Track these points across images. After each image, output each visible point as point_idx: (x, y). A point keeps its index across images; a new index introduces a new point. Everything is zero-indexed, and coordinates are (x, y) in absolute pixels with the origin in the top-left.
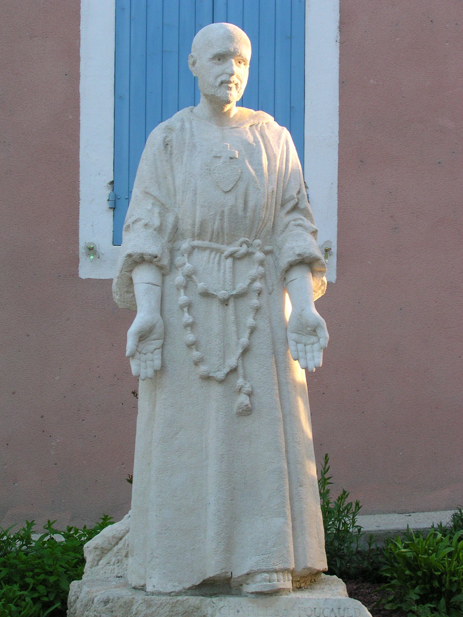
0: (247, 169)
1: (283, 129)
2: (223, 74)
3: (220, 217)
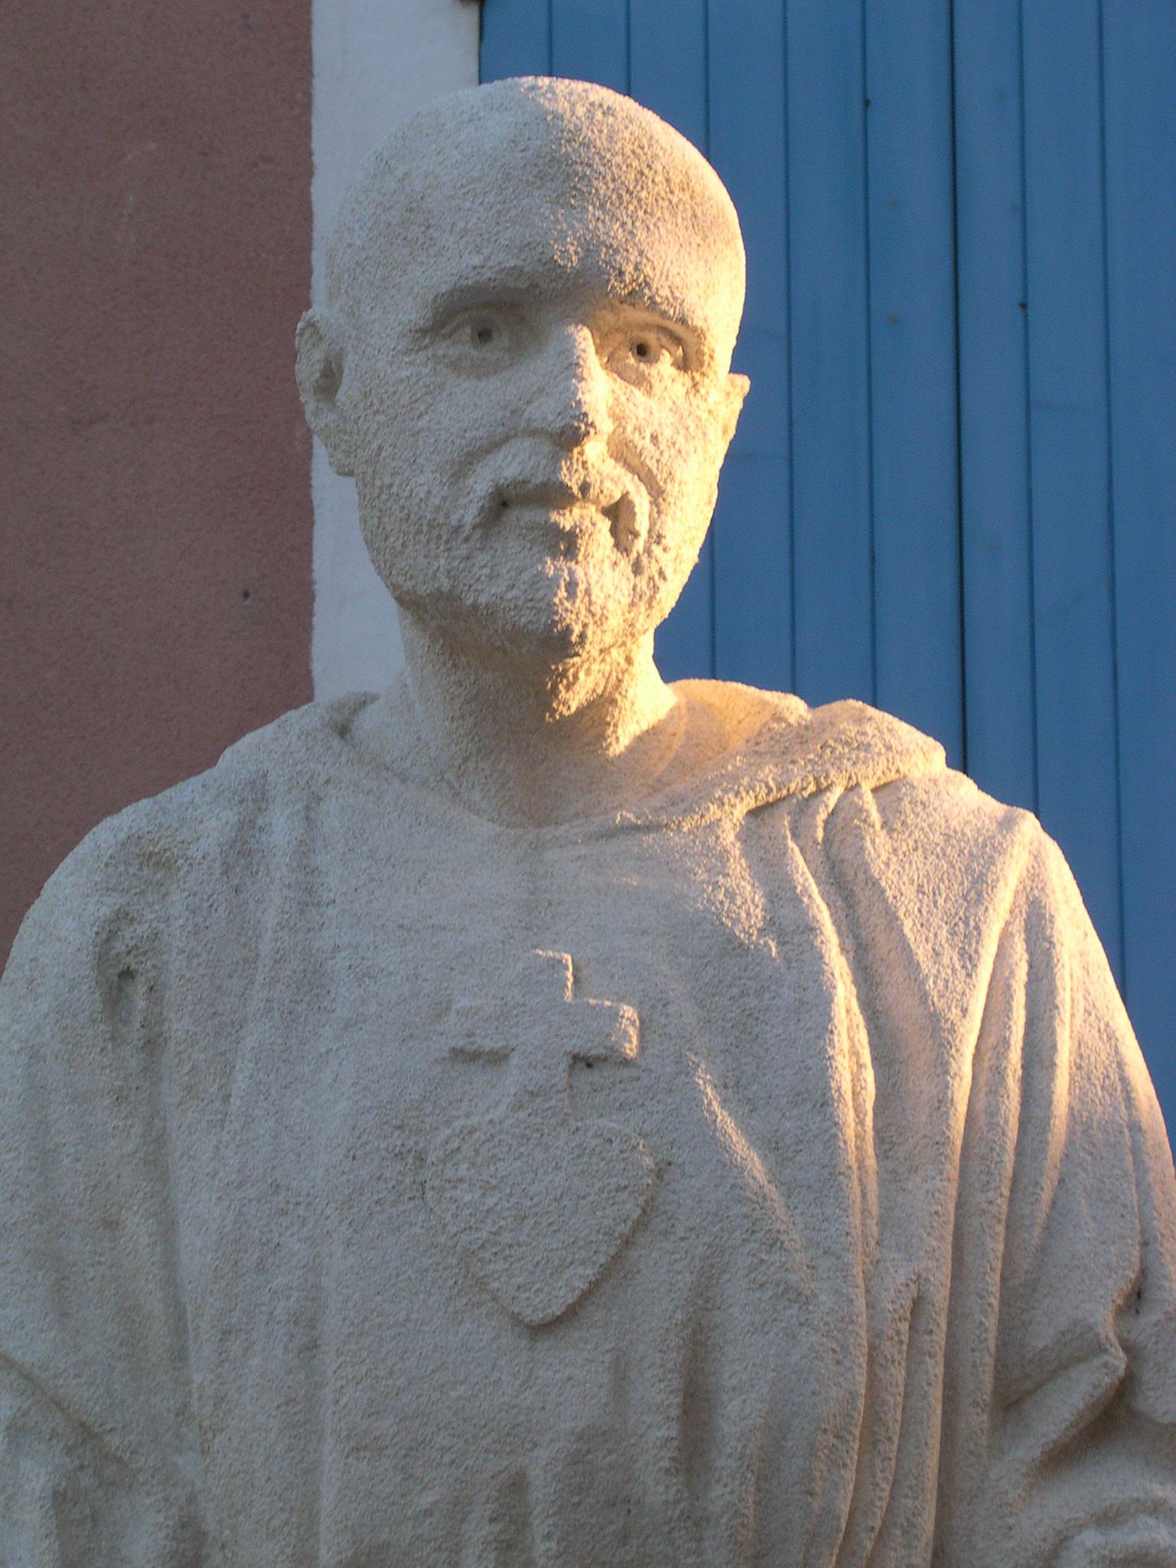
0: (709, 1137)
1: (1007, 825)
2: (507, 439)
3: (497, 1527)
